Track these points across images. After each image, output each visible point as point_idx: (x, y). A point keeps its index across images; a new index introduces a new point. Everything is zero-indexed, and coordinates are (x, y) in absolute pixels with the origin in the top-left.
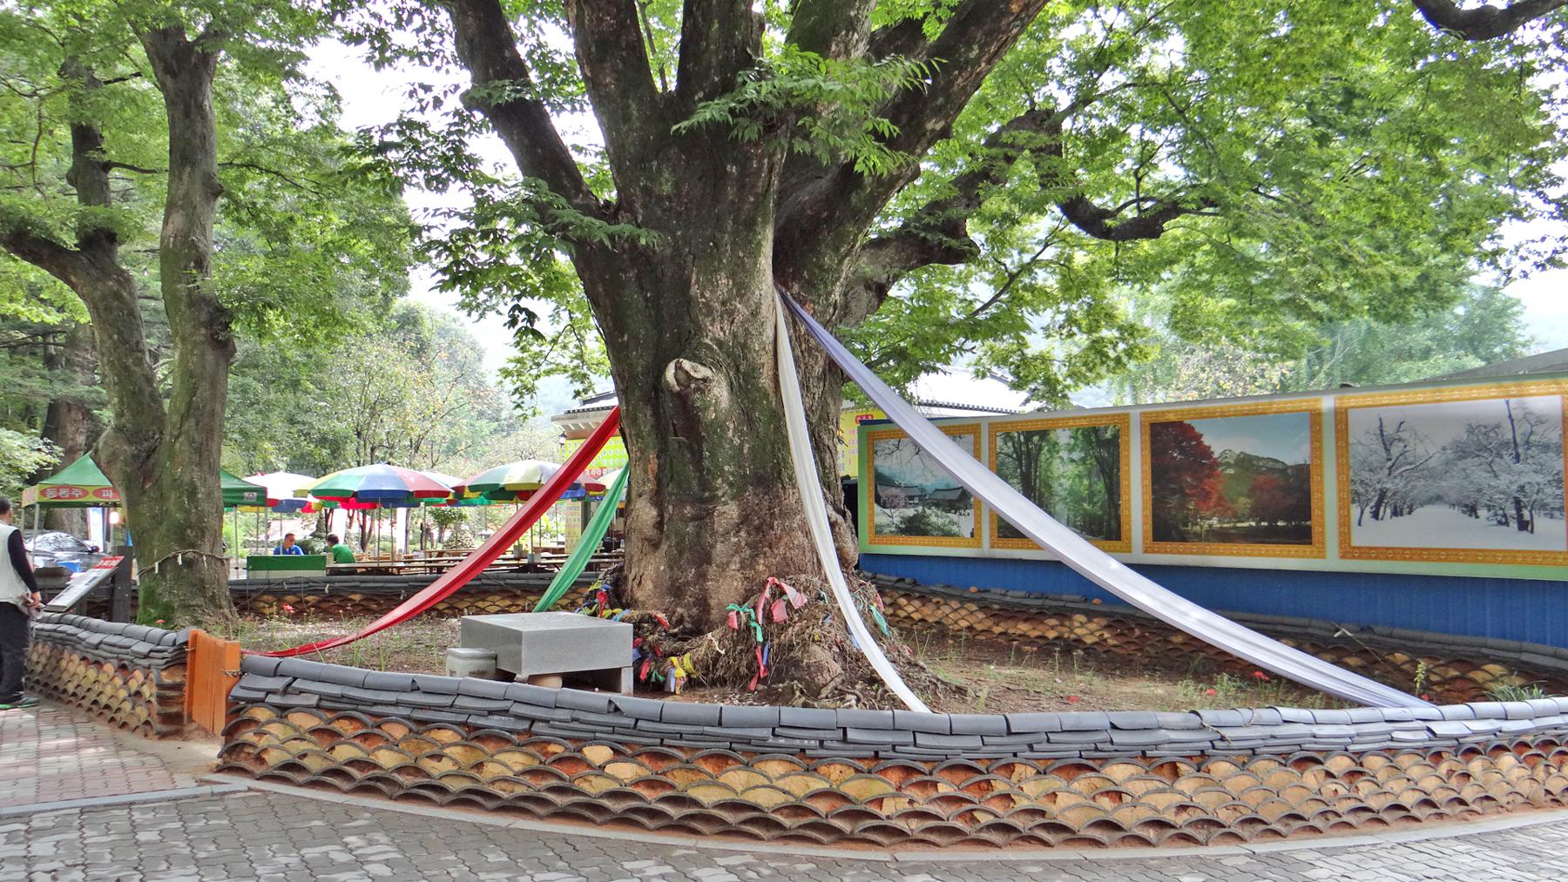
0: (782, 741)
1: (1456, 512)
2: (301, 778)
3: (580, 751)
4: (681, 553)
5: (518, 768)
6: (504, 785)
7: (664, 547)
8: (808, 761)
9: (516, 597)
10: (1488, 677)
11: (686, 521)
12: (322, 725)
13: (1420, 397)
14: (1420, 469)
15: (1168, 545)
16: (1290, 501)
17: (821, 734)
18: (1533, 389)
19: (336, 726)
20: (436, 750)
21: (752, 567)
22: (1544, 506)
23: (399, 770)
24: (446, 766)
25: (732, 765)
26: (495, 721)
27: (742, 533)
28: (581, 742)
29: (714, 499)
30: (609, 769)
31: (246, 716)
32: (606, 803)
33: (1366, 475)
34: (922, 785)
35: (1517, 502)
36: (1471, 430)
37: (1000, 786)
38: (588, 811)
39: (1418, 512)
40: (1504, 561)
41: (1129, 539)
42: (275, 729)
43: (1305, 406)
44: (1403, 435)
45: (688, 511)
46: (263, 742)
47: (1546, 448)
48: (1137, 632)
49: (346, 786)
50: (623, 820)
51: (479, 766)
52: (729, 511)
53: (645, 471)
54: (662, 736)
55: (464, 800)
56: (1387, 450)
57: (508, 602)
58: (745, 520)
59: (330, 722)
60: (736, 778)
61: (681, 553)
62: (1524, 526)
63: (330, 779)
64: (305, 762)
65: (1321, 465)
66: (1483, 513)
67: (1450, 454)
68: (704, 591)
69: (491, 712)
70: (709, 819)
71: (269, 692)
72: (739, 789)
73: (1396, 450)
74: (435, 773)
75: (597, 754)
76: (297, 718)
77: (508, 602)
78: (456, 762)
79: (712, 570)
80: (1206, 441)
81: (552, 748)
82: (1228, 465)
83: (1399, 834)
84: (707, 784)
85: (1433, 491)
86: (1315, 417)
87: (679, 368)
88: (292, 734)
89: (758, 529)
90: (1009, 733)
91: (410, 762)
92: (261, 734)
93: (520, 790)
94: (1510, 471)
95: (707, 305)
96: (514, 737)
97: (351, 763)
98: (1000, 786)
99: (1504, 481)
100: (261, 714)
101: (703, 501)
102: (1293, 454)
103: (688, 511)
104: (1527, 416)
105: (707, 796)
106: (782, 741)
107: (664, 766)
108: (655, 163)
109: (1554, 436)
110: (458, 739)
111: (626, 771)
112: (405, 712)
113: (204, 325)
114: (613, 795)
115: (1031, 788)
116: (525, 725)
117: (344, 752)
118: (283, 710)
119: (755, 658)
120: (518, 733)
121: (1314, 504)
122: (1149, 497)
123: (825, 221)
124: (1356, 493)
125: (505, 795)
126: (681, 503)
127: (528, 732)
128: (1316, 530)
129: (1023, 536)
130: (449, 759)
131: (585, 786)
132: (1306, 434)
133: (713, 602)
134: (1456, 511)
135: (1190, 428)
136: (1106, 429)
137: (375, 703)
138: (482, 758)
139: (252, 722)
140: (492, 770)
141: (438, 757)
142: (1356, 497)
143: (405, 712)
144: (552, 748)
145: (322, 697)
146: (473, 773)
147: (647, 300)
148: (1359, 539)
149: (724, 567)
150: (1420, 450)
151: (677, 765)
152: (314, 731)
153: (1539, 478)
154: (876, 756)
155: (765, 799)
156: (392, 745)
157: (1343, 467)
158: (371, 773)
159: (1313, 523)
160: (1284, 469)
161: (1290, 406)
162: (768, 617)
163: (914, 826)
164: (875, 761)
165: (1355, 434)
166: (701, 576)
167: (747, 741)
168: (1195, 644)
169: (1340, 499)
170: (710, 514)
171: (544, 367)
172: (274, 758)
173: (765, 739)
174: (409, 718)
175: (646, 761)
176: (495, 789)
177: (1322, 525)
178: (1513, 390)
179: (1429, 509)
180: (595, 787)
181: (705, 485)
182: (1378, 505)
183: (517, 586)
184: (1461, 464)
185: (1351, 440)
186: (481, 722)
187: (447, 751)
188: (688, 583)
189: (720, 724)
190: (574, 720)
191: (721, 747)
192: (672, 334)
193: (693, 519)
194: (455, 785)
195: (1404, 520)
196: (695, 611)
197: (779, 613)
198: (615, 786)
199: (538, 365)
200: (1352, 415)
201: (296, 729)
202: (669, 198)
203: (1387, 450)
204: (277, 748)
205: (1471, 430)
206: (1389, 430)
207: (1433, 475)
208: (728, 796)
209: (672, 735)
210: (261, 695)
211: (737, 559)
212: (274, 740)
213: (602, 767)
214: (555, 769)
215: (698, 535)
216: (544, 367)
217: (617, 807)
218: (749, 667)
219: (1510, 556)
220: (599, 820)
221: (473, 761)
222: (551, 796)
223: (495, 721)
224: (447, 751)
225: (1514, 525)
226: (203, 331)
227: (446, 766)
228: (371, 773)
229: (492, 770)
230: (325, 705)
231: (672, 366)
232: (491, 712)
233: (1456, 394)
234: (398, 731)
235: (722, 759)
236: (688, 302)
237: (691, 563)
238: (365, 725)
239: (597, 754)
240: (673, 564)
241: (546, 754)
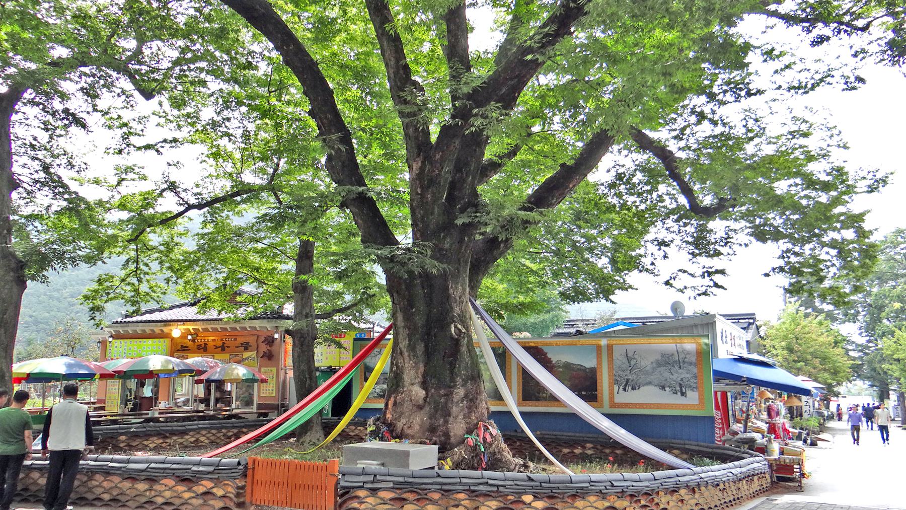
1: (657, 389)
4: (436, 411)
9: (166, 437)
10: (164, 488)
12: (397, 496)
15: (530, 403)
16: (588, 383)
18: (686, 341)
19: (404, 496)
20: (456, 503)
21: (469, 417)
22: (690, 386)
26: (481, 488)
30: (533, 504)
31: (353, 495)
33: (621, 373)
34: (636, 502)
35: (680, 385)
36: (663, 355)
37: (656, 500)
39: (642, 388)
42: (371, 500)
43: (594, 342)
45: (442, 392)
47: (691, 364)
48: (518, 443)
52: (460, 392)
54: (551, 489)
57: (161, 441)
62: (683, 394)
66: (667, 389)
68: (447, 428)
69: (480, 484)
71: (364, 482)
73: (633, 363)
75: (528, 498)
76: (382, 494)
77: (161, 441)
80: (549, 356)
81: (509, 497)
82: (559, 367)
85: (648, 380)
86: (599, 348)
87: (456, 327)
88: (379, 501)
89: (471, 400)
94: (677, 372)
98: (656, 500)
99: (675, 377)
100: (361, 493)
101: (450, 387)
102: (589, 363)
103: (442, 392)
104: (683, 350)
107: (554, 501)
109: (694, 359)
110: (467, 497)
112: (439, 487)
113: (12, 270)
115: (664, 500)
118: (374, 491)
121: (598, 385)
123: (484, 261)
126: (438, 388)
127: (498, 491)
128: (599, 395)
129: (558, 400)
133: (452, 434)
137: (423, 484)
138: (479, 504)
142: (617, 382)
143: (439, 487)
144: (509, 497)
145: (394, 483)
150: (643, 363)
152: (391, 500)
153: (688, 376)
154: (623, 491)
157: (611, 368)
162: (485, 439)
165: (616, 355)
166: (446, 422)
167: (582, 488)
168: (616, 445)
169: (610, 383)
170: (452, 394)
171: (112, 295)
174: (441, 489)
178: (678, 341)
179: (646, 387)
181: (453, 380)
183: (167, 431)
184: (659, 369)
186: (476, 488)
189: (571, 482)
191: (573, 492)
192: (438, 310)
193: (444, 395)
197: (489, 439)
199: (108, 294)
200: (614, 347)
201: (381, 499)
202: (446, 250)
205: (663, 355)
207: (647, 373)
210: (361, 484)
213: (530, 504)
215: (446, 403)
216: (112, 295)
218: (478, 463)
219: (678, 406)
223: (481, 488)
225: (679, 394)
226: (12, 274)
230: (398, 486)
231: (453, 326)
232: (480, 484)
233: (656, 341)
236: (448, 297)
237: (442, 416)
238: (420, 494)
241: (507, 500)
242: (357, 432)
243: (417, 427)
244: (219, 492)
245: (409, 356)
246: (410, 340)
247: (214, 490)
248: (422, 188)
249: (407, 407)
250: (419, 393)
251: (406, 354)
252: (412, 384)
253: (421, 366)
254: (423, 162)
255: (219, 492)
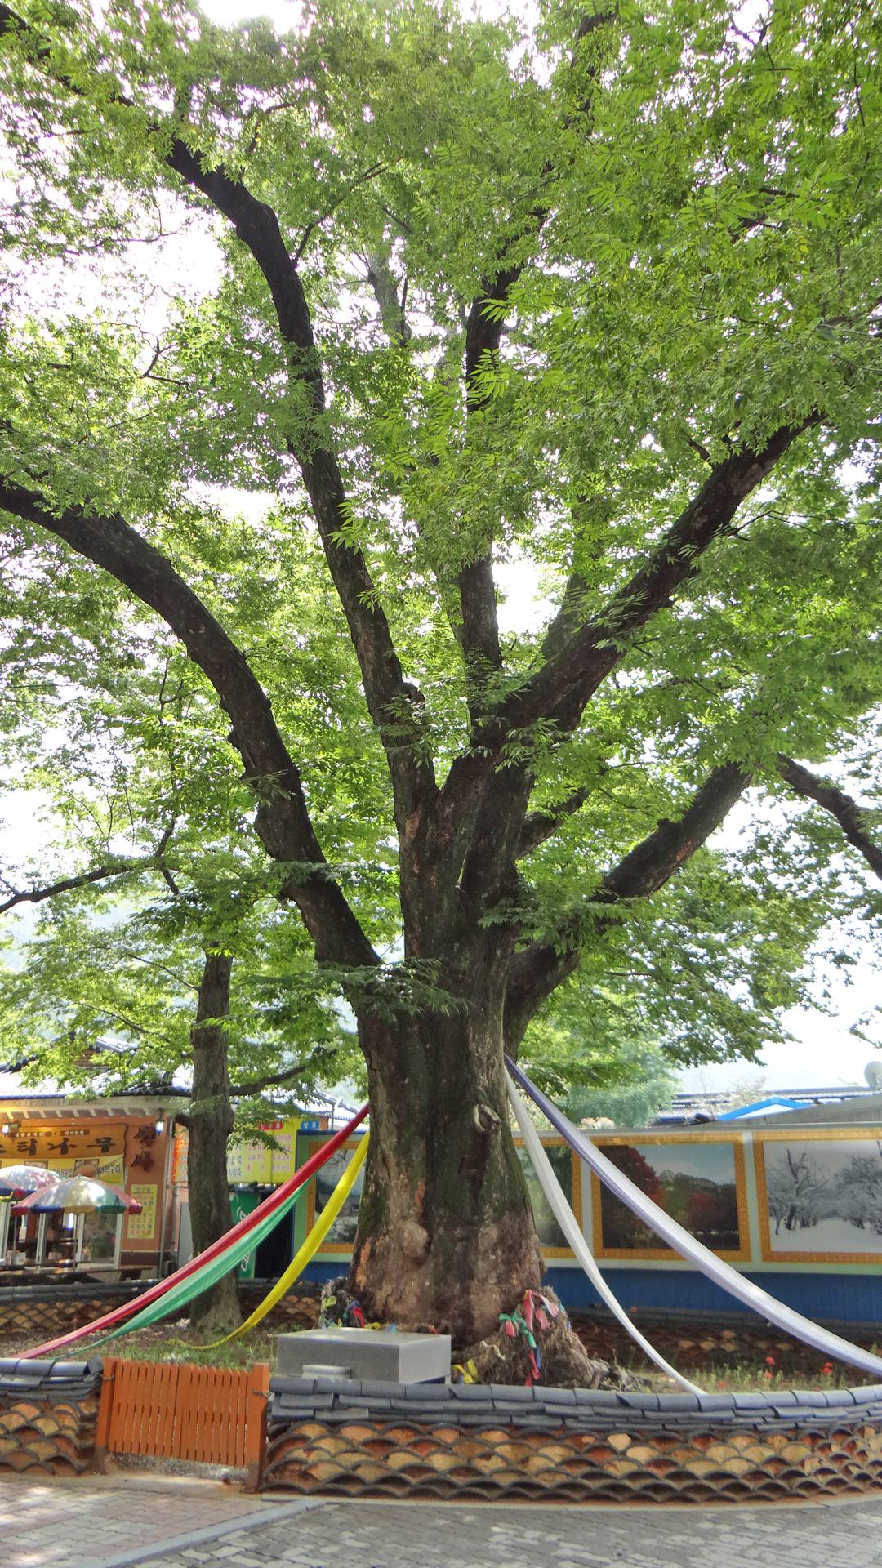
0: (741, 1420)
2: (354, 1489)
3: (606, 1440)
5: (558, 1459)
6: (546, 1476)
7: (431, 1265)
8: (759, 1435)
11: (455, 1241)
12: (376, 1436)
13: (817, 1136)
14: (820, 1192)
15: (617, 1251)
17: (761, 1413)
19: (390, 1436)
23: (453, 1471)
24: (495, 1463)
25: (714, 1442)
26: (533, 1420)
27: (499, 1252)
28: (604, 1433)
29: (481, 1221)
31: (296, 1433)
32: (627, 1483)
33: (779, 1195)
36: (855, 1162)
38: (615, 1492)
40: (804, 1261)
41: (749, 1248)
42: (327, 1444)
44: (806, 1164)
45: (458, 1232)
46: (313, 1457)
48: (597, 1330)
49: (398, 1492)
50: (639, 1498)
51: (525, 1461)
52: (491, 1232)
53: (412, 1196)
55: (511, 1494)
56: (795, 1175)
58: (502, 1240)
59: (384, 1432)
60: (717, 1452)
61: (448, 1269)
63: (384, 1487)
64: (360, 1472)
65: (744, 1186)
66: (867, 1225)
67: (841, 1179)
68: (468, 1303)
69: (529, 1413)
70: (699, 1489)
71: (316, 1409)
72: (720, 1461)
73: (801, 1175)
74: (486, 1471)
78: (504, 1459)
79: (474, 1284)
80: (649, 1162)
82: (668, 1184)
83: (745, 1511)
84: (699, 1460)
86: (738, 1148)
88: (343, 1446)
90: (856, 1403)
91: (463, 1462)
92: (310, 1450)
93: (560, 1479)
95: (479, 1059)
96: (554, 1433)
97: (404, 1469)
98: (861, 1446)
100: (311, 1431)
102: (722, 1176)
105: (699, 1469)
106: (741, 1420)
108: (457, 945)
110: (506, 1438)
111: (642, 1454)
114: (633, 1476)
116: (558, 1423)
117: (398, 1460)
118: (334, 1427)
119: (529, 1361)
120: (556, 1428)
122: (599, 1210)
124: (773, 1208)
125: (548, 1485)
126: (450, 1226)
128: (742, 1238)
130: (497, 1457)
131: (611, 1470)
132: (731, 1161)
133: (476, 1313)
134: (848, 1223)
135: (634, 1152)
136: (559, 1149)
138: (527, 1452)
139: (304, 1439)
140: (537, 1463)
141: (487, 1456)
142: (773, 1212)
145: (372, 1410)
146: (520, 1467)
147: (426, 1051)
148: (777, 1245)
149: (484, 1281)
150: (819, 1176)
151: (678, 1445)
152: (366, 1443)
155: (737, 1467)
156: (445, 1449)
158: (425, 1477)
159: (741, 1232)
160: (714, 1189)
161: (717, 1138)
162: (536, 1323)
163: (821, 1480)
164: (795, 1433)
166: (466, 1290)
167: (720, 1422)
170: (476, 1236)
172: (324, 1472)
173: (730, 1419)
175: (653, 1443)
176: (539, 1480)
177: (747, 1234)
180: (619, 1470)
181: (477, 1210)
182: (790, 1219)
184: (850, 1187)
185: (767, 1166)
186: (523, 1421)
187: (497, 1450)
188: (453, 1298)
190: (597, 1414)
193: (462, 1239)
194: (506, 1480)
195: (811, 1230)
196: (460, 1322)
198: (635, 1468)
200: (766, 1147)
201: (348, 1441)
202: (464, 973)
203: (795, 1175)
204: (328, 1462)
205: (855, 1162)
206: (796, 1160)
207: (828, 1195)
208: (713, 1468)
209: (668, 1420)
210: (310, 1413)
211: (494, 1274)
212: (325, 1455)
213: (624, 1453)
214: (588, 1457)
215: (465, 1254)
217: (636, 1485)
218: (524, 1370)
220: (619, 1497)
221: (521, 1457)
222: (585, 1482)
223: (533, 1420)
224: (497, 1450)
227: (495, 1463)
228: (425, 1477)
229: (537, 1463)
230: (379, 1417)
232: (529, 1413)
234: (449, 1437)
235: (706, 1438)
236: (467, 1056)
239: (619, 1441)
240: (439, 1279)
242: (301, 1307)
243: (412, 1301)
244: (48, 1427)
245: (398, 1164)
246: (400, 1136)
247: (40, 1424)
248: (420, 864)
249: (394, 1262)
250: (417, 1235)
251: (392, 1161)
252: (404, 1218)
253: (421, 1183)
254: (423, 822)
255: (48, 1427)
